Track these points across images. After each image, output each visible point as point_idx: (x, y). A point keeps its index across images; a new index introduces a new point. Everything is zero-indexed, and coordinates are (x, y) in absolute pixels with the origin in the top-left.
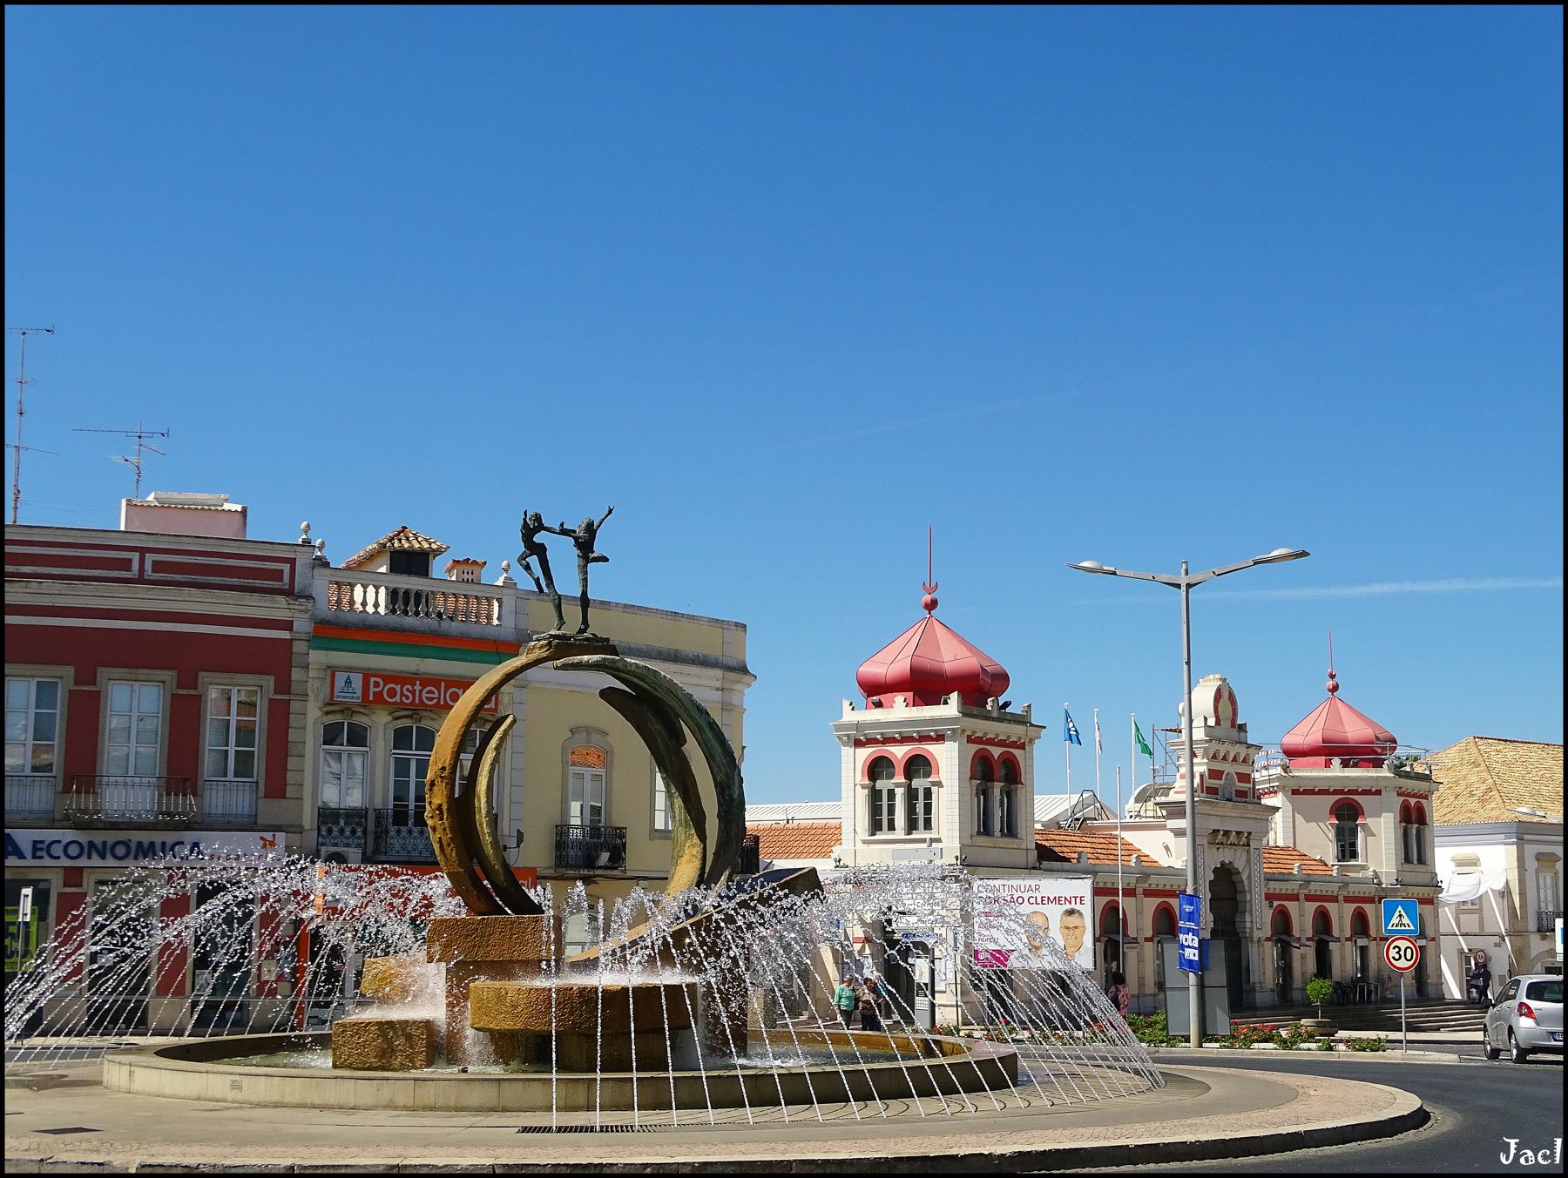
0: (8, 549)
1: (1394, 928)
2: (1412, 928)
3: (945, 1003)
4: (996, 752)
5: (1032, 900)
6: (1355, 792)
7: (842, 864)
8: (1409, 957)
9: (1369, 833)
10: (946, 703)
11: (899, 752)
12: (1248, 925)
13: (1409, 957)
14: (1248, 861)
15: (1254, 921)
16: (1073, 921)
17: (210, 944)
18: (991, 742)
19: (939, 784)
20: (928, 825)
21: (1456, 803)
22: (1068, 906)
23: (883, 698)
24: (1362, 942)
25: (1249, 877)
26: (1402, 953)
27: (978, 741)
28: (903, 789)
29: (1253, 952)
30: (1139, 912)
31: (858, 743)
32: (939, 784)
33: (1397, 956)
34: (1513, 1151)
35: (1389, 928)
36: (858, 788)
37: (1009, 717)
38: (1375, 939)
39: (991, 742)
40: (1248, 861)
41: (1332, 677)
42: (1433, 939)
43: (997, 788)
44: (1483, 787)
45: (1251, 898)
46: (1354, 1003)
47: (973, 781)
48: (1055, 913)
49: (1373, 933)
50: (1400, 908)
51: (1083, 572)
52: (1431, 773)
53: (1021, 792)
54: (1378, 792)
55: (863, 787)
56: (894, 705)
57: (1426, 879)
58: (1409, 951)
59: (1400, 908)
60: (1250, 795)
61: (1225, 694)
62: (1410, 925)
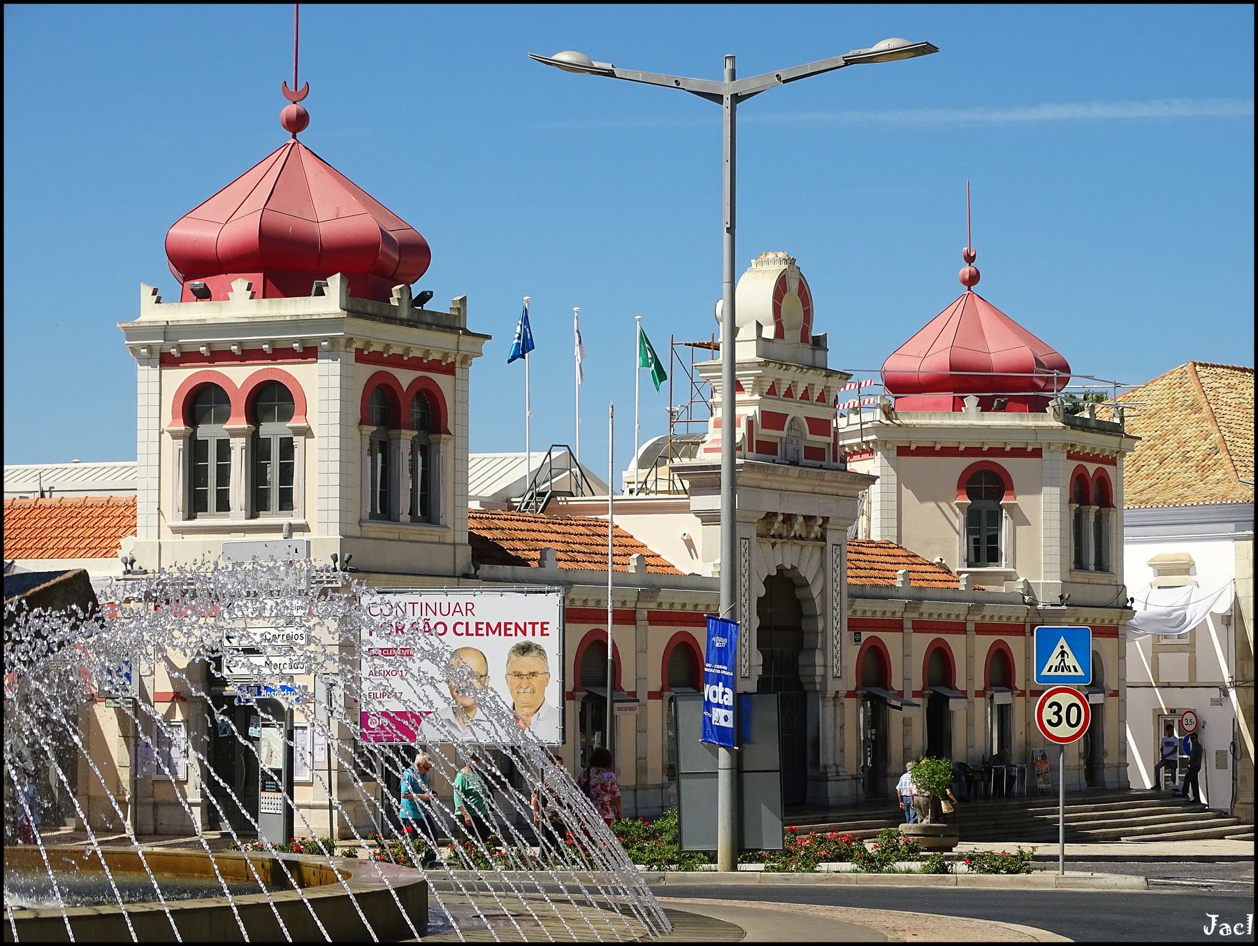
1: (1052, 673)
2: (1080, 673)
3: (312, 802)
4: (405, 378)
5: (461, 629)
6: (999, 452)
8: (1073, 721)
9: (1020, 519)
10: (320, 293)
11: (239, 376)
12: (819, 671)
13: (1073, 721)
14: (823, 565)
15: (829, 663)
16: (528, 663)
18: (397, 361)
19: (306, 432)
20: (286, 502)
21: (1162, 470)
22: (521, 639)
24: (1001, 698)
25: (823, 591)
26: (1063, 714)
27: (375, 358)
28: (243, 440)
29: (826, 715)
30: (641, 650)
32: (306, 432)
33: (1055, 719)
34: (1214, 925)
35: (1045, 672)
36: (167, 437)
37: (429, 319)
38: (1023, 694)
39: (397, 361)
40: (823, 565)
41: (970, 259)
42: (1116, 693)
43: (406, 439)
44: (1205, 446)
45: (825, 627)
46: (986, 796)
47: (365, 427)
48: (498, 650)
49: (1019, 683)
50: (1062, 641)
52: (1122, 419)
53: (446, 447)
54: (1037, 453)
55: (175, 436)
56: (230, 294)
57: (1107, 595)
58: (1074, 710)
59: (1062, 641)
60: (829, 456)
61: (793, 286)
62: (1078, 668)
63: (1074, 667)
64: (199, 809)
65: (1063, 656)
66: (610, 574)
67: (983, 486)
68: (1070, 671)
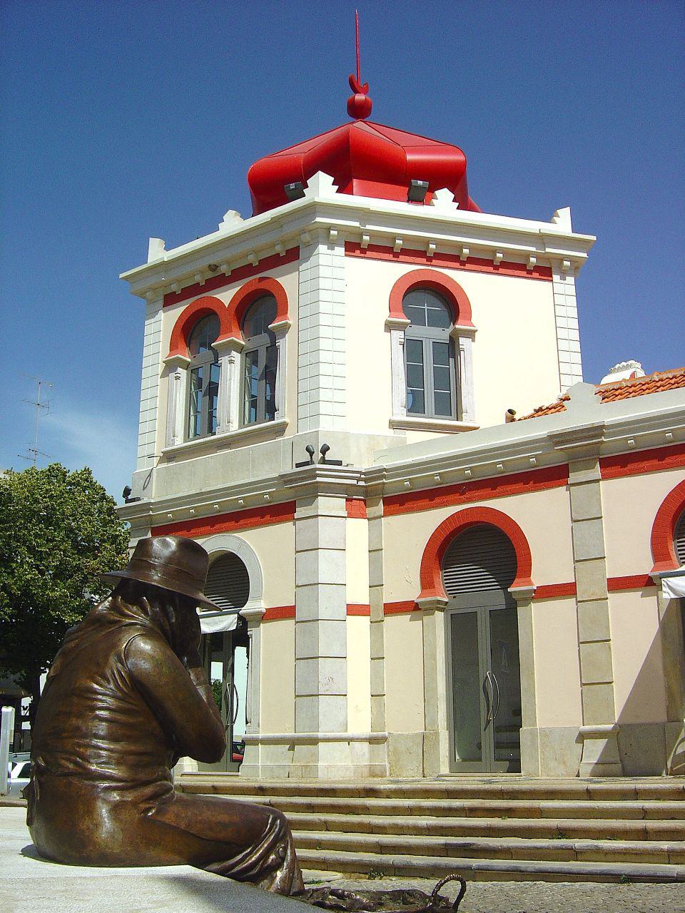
23: (210, 275)
31: (170, 300)
67: (426, 307)
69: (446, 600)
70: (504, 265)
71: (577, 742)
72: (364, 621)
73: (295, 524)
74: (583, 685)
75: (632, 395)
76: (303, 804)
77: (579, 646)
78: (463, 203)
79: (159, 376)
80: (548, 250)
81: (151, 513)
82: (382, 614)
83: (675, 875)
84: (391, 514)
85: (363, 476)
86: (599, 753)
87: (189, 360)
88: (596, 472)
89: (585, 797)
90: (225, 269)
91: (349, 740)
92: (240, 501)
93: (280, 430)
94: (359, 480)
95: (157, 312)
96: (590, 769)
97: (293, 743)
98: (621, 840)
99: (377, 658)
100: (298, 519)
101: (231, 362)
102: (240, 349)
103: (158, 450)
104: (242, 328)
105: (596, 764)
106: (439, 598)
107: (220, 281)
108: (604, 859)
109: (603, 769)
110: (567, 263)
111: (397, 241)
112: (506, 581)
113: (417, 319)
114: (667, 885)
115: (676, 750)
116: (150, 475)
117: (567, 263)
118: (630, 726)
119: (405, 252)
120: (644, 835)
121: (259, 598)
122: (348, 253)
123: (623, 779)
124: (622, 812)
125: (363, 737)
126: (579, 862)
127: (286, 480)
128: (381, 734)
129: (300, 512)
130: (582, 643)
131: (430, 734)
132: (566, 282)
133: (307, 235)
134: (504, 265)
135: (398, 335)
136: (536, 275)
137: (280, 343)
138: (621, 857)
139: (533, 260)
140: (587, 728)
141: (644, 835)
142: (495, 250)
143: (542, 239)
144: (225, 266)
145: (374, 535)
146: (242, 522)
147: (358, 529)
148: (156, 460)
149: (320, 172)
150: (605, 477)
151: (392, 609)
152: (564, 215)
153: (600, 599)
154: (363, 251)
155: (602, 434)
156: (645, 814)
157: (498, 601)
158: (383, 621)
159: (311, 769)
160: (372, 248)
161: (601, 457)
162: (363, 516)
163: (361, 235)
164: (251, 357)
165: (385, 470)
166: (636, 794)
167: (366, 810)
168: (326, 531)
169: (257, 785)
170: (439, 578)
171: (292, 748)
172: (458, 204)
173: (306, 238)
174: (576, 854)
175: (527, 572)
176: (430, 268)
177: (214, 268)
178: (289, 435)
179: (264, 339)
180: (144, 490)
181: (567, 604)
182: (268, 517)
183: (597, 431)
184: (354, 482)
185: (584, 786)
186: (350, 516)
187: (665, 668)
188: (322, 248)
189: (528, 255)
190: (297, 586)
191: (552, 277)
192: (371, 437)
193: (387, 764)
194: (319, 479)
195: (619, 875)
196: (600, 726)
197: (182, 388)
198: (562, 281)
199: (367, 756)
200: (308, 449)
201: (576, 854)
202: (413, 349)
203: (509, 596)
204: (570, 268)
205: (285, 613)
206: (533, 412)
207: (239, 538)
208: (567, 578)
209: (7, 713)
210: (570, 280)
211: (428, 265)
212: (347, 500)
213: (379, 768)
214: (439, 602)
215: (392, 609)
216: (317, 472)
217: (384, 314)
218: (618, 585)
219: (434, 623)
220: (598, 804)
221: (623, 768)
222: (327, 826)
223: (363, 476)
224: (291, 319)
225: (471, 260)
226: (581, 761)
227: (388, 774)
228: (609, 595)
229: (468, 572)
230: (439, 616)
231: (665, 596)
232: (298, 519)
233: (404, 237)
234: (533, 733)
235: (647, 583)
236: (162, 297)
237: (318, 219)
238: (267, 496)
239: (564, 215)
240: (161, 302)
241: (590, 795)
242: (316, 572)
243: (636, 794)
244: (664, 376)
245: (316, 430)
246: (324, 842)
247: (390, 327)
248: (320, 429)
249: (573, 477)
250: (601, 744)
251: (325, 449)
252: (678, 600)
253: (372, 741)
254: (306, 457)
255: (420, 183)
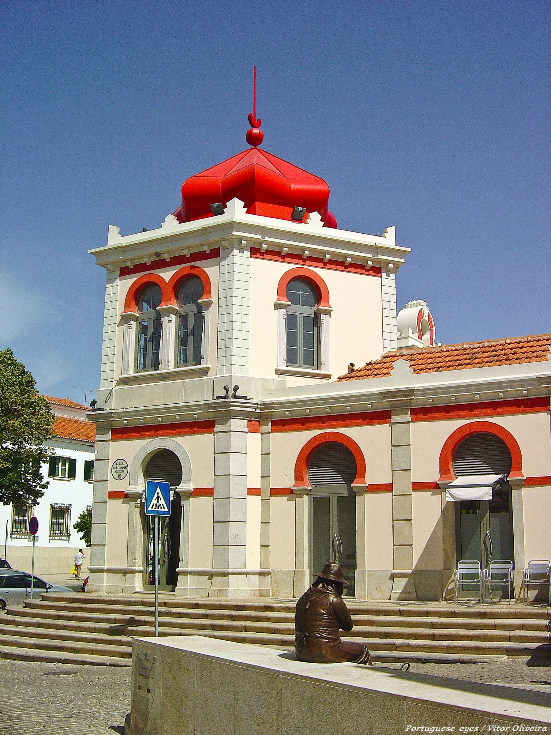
0: (293, 626)
1: (153, 509)
2: (166, 510)
7: (96, 407)
17: (23, 508)
23: (155, 259)
31: (125, 272)
50: (158, 490)
51: (7, 541)
59: (158, 490)
63: (163, 505)
64: (27, 589)
65: (158, 499)
66: (509, 593)
67: (300, 293)
68: (161, 509)
69: (310, 488)
70: (352, 265)
71: (390, 579)
72: (257, 499)
73: (214, 435)
74: (394, 545)
75: (430, 371)
76: (228, 615)
77: (393, 522)
78: (329, 222)
79: (117, 325)
80: (380, 257)
81: (112, 419)
82: (269, 495)
83: (451, 659)
84: (275, 432)
85: (259, 406)
86: (403, 587)
87: (138, 315)
88: (408, 417)
89: (181, 494)
90: (166, 257)
91: (247, 574)
92: (177, 418)
93: (205, 372)
94: (256, 408)
95: (115, 280)
96: (397, 595)
97: (211, 575)
98: (420, 639)
99: (265, 522)
100: (216, 432)
101: (170, 321)
102: (176, 313)
103: (117, 376)
104: (177, 298)
105: (401, 593)
106: (307, 488)
107: (162, 264)
108: (411, 650)
109: (405, 596)
110: (391, 266)
111: (284, 249)
112: (349, 480)
113: (294, 300)
114: (446, 664)
115: (448, 586)
116: (110, 393)
117: (391, 266)
118: (421, 571)
119: (289, 255)
120: (433, 637)
121: (189, 481)
122: (252, 255)
123: (417, 603)
124: (420, 624)
125: (256, 572)
126: (397, 652)
127: (209, 406)
128: (267, 570)
129: (218, 428)
130: (395, 520)
131: (299, 571)
132: (390, 278)
133: (226, 242)
134: (352, 265)
135: (283, 312)
136: (371, 272)
137: (205, 313)
138: (422, 650)
139: (370, 263)
140: (396, 571)
141: (433, 637)
142: (346, 256)
143: (376, 249)
144: (167, 254)
145: (265, 444)
146: (177, 431)
147: (255, 439)
148: (114, 383)
149: (235, 198)
150: (413, 420)
151: (276, 492)
152: (391, 231)
153: (406, 495)
154: (262, 254)
155: (413, 395)
156: (433, 625)
157: (343, 491)
158: (270, 499)
159: (223, 592)
160: (268, 252)
161: (411, 408)
162: (258, 432)
163: (261, 244)
164: (183, 320)
165: (274, 403)
166: (427, 614)
167: (268, 619)
168: (235, 441)
169: (194, 602)
170: (306, 474)
171: (210, 578)
172: (323, 223)
173: (225, 244)
174: (396, 647)
175: (363, 475)
176: (304, 267)
177: (158, 254)
178: (211, 376)
179: (191, 308)
180: (106, 403)
181: (386, 497)
182: (195, 429)
183: (410, 392)
184: (253, 410)
185: (397, 608)
186: (250, 431)
187: (444, 538)
188: (236, 252)
189: (367, 259)
190: (215, 476)
191: (381, 274)
192: (264, 380)
193: (270, 589)
194: (232, 408)
195: (421, 659)
196: (403, 571)
197: (133, 334)
198: (387, 277)
199: (257, 584)
200: (225, 388)
201: (396, 647)
202: (291, 321)
203: (350, 489)
204: (394, 268)
205: (208, 492)
206: (365, 364)
207: (175, 441)
208: (387, 480)
209: (134, 582)
210: (393, 276)
211: (303, 265)
212: (249, 421)
213: (265, 591)
214: (307, 490)
215: (276, 492)
216: (231, 403)
217: (273, 297)
218: (418, 486)
219: (303, 503)
220: (407, 619)
221: (417, 595)
222: (246, 629)
223: (259, 406)
224: (214, 297)
225: (331, 262)
226: (392, 591)
227: (271, 595)
228: (412, 493)
229: (323, 471)
230: (306, 498)
231: (448, 499)
232: (216, 432)
233: (289, 246)
234: (363, 573)
235: (435, 487)
236: (119, 269)
237: (234, 233)
238: (196, 416)
239: (391, 231)
240: (118, 273)
241: (401, 613)
242: (229, 468)
243: (427, 614)
244: (450, 349)
245: (230, 375)
246: (247, 639)
247: (277, 306)
248: (232, 374)
249: (394, 419)
250: (404, 581)
251: (236, 388)
252: (453, 502)
253: (261, 574)
254: (224, 393)
255: (300, 209)
